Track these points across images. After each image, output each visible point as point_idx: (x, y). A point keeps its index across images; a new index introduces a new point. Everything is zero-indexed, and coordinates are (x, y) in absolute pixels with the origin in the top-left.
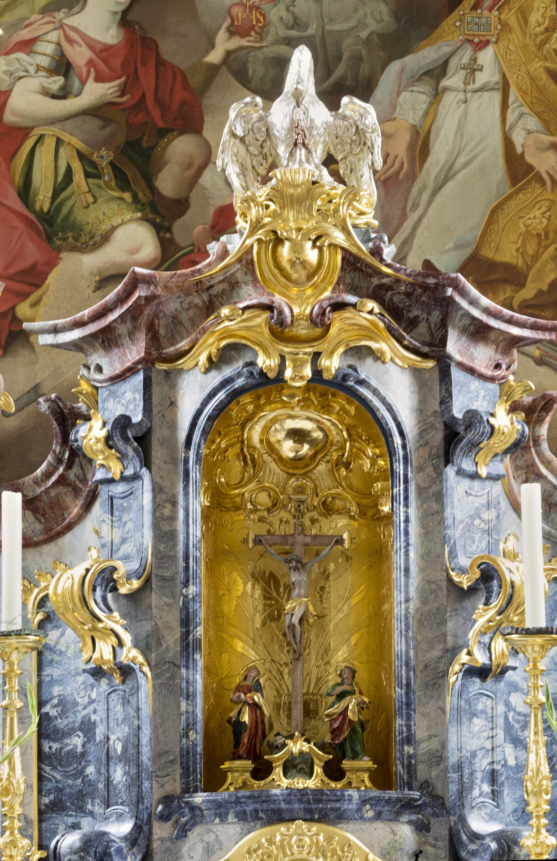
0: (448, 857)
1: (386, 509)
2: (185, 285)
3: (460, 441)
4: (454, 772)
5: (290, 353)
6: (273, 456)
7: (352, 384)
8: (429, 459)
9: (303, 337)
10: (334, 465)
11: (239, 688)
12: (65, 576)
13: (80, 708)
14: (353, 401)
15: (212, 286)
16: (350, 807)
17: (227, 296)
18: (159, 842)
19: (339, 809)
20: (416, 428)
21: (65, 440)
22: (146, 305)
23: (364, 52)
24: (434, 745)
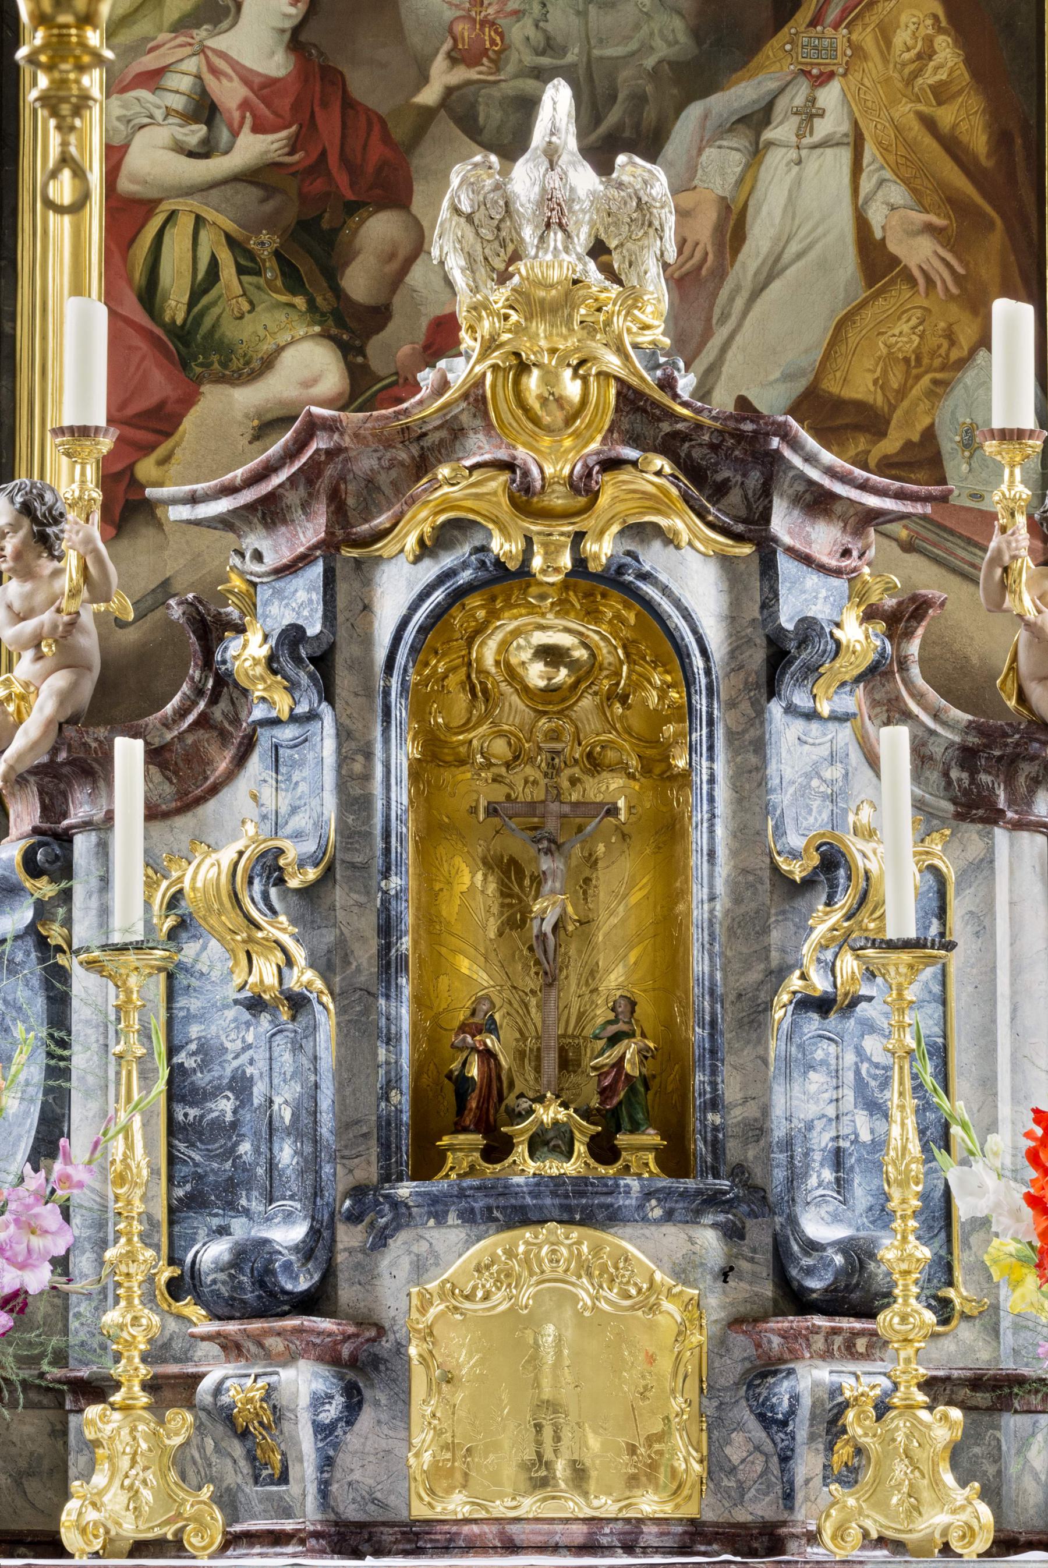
1: (681, 763)
3: (790, 663)
4: (781, 1152)
5: (539, 533)
7: (631, 578)
11: (463, 1028)
12: (208, 862)
13: (230, 1056)
15: (424, 435)
16: (627, 1202)
18: (347, 1254)
19: (612, 1205)
21: (208, 662)
22: (327, 463)
23: (649, 89)
24: (751, 1111)
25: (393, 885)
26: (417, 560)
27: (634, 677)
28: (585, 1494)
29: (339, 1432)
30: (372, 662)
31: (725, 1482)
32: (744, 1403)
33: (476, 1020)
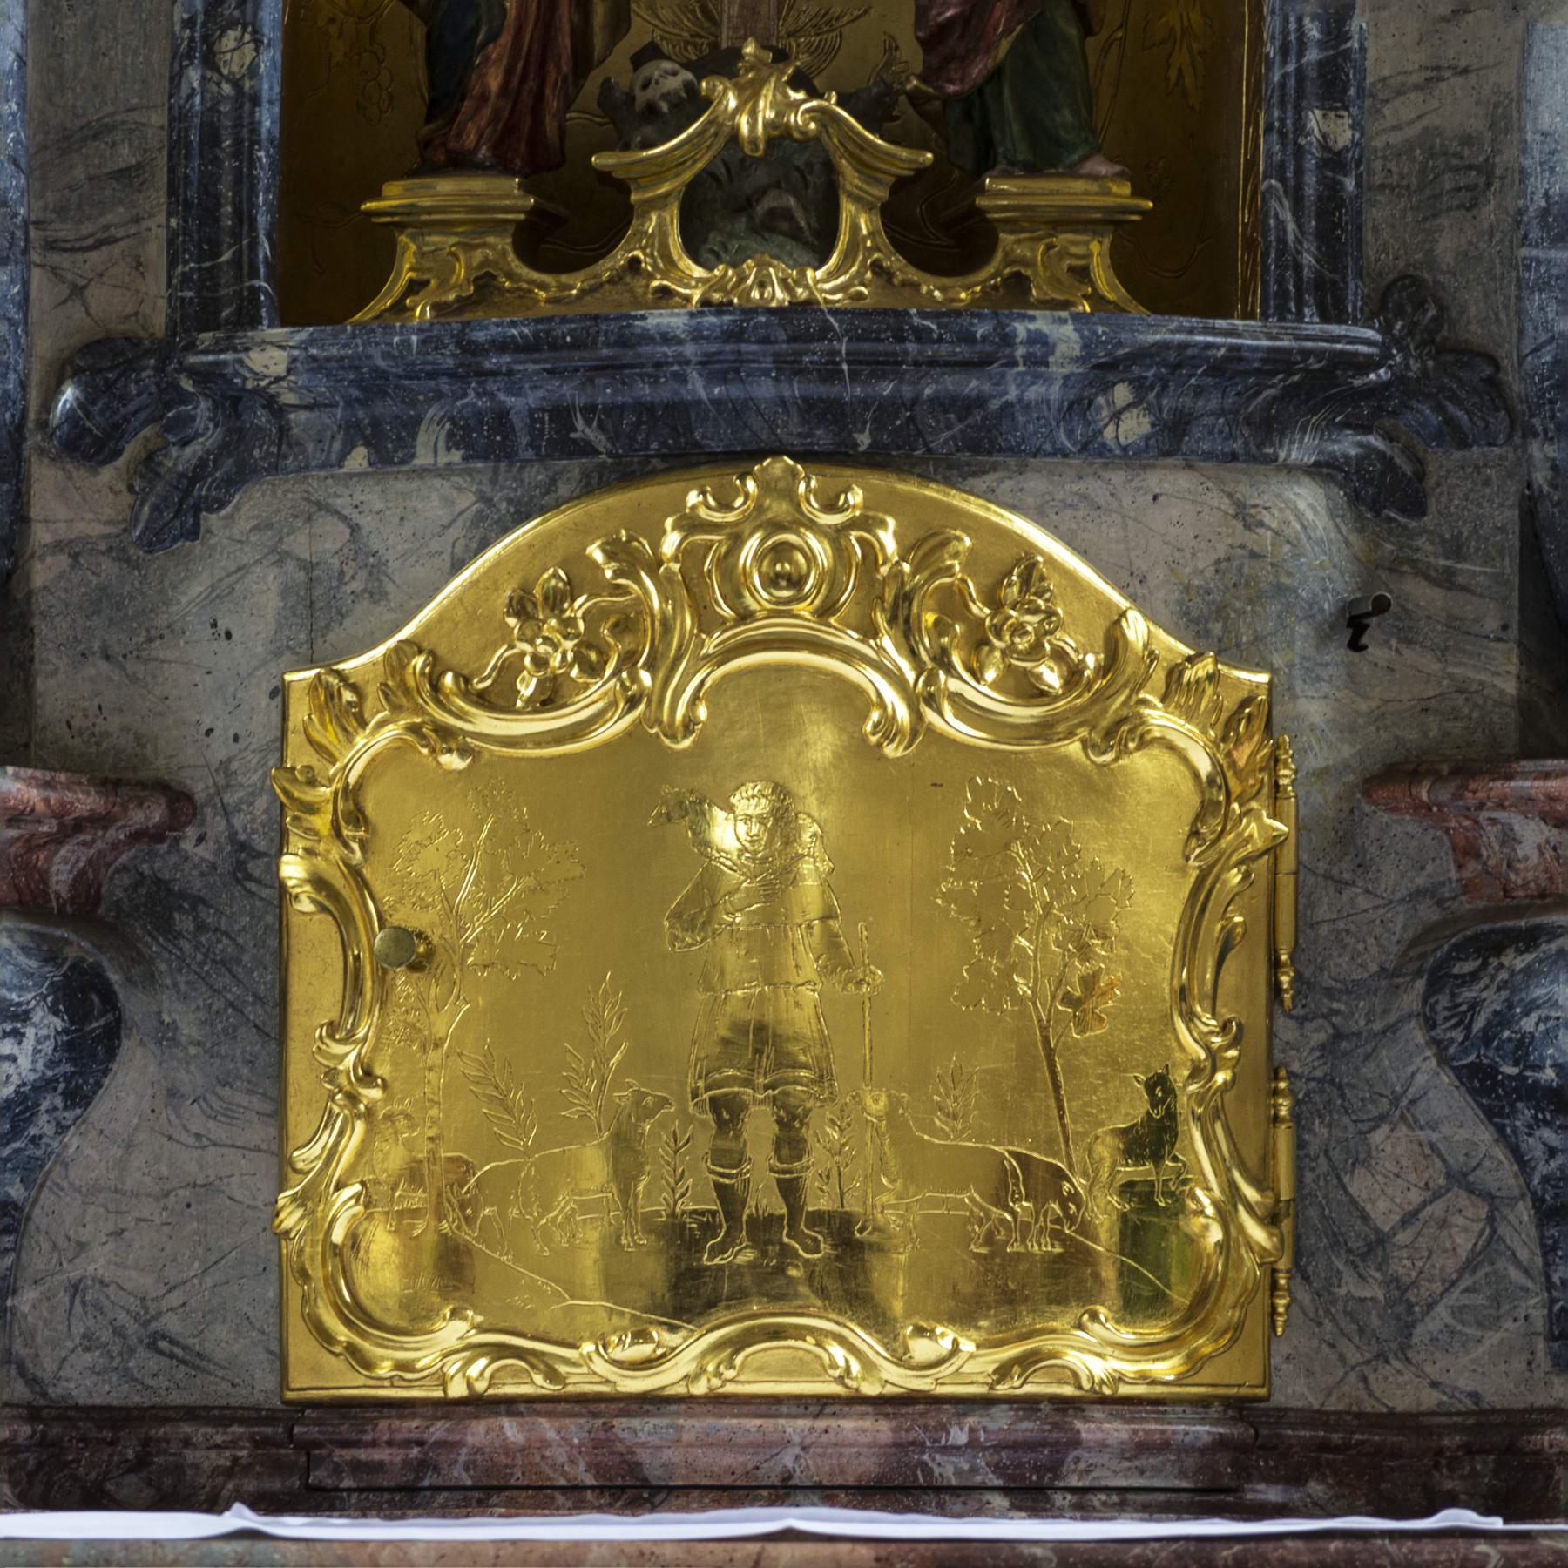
0: (1514, 632)
16: (1034, 392)
18: (63, 561)
19: (981, 401)
28: (879, 1321)
29: (43, 1125)
31: (1350, 1286)
32: (1416, 1034)
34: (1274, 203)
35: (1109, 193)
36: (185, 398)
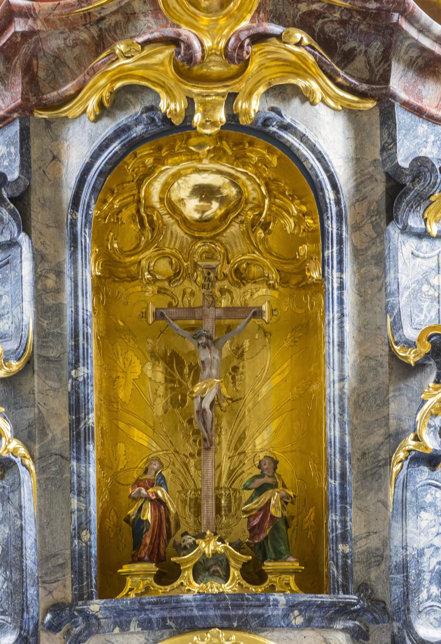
1: (316, 275)
2: (70, 18)
3: (406, 194)
4: (398, 573)
5: (198, 95)
6: (175, 217)
7: (275, 129)
8: (367, 215)
9: (215, 75)
10: (250, 227)
11: (138, 483)
14: (275, 150)
15: (103, 18)
16: (275, 613)
17: (121, 29)
19: (263, 615)
20: (352, 180)
25: (81, 374)
26: (97, 119)
27: (274, 208)
30: (61, 201)
33: (148, 476)
34: (331, 567)
35: (294, 565)
36: (76, 617)
